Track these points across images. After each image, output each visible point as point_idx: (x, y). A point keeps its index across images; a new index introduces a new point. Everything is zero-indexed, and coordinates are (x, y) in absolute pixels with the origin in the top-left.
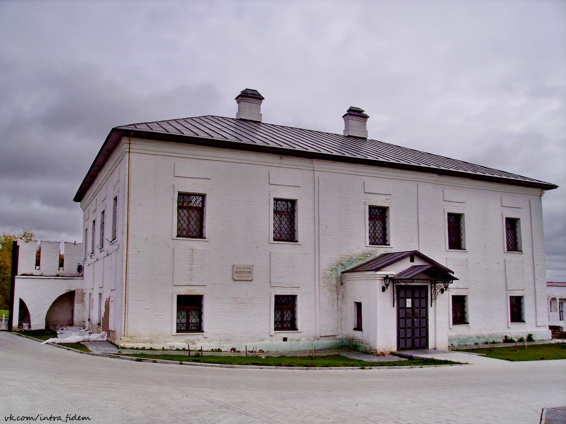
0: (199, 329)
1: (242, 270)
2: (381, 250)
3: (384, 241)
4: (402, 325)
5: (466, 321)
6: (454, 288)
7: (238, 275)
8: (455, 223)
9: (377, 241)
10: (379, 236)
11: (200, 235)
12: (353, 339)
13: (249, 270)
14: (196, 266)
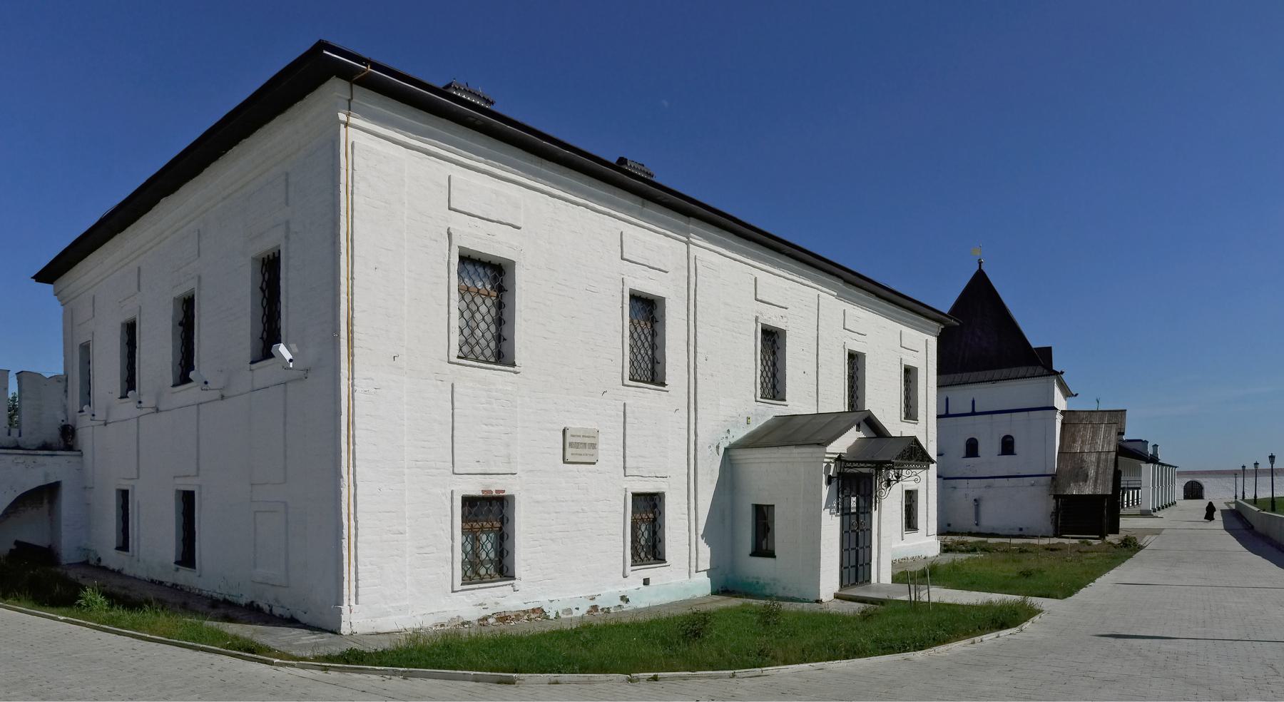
2: (777, 410)
7: (574, 450)
11: (502, 355)
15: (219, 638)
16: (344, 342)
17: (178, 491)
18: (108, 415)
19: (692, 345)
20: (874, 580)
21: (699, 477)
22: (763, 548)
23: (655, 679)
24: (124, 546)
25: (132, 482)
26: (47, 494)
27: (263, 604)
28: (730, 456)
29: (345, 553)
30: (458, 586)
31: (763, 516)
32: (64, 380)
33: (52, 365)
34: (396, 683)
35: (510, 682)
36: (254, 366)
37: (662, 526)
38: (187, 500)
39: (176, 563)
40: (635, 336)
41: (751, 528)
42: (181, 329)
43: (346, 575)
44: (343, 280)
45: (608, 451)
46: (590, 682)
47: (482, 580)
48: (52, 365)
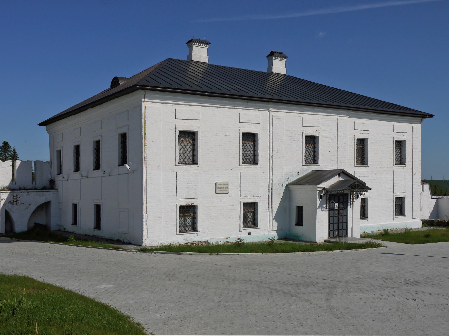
0: (194, 229)
2: (314, 168)
3: (315, 161)
4: (332, 222)
5: (366, 216)
6: (366, 195)
7: (220, 190)
8: (362, 144)
10: (312, 156)
11: (194, 162)
12: (9, 277)
13: (227, 186)
14: (194, 185)
15: (109, 247)
16: (144, 163)
17: (95, 205)
18: (68, 177)
19: (271, 148)
20: (349, 235)
21: (273, 196)
22: (299, 222)
23: (217, 254)
24: (75, 223)
25: (78, 201)
26: (46, 206)
27: (122, 240)
28: (288, 189)
29: (144, 223)
30: (178, 233)
31: (300, 209)
32: (50, 163)
33: (46, 157)
34: (153, 254)
35: (180, 254)
36: (119, 167)
37: (257, 214)
38: (98, 208)
39: (94, 228)
40: (245, 150)
41: (293, 215)
42: (95, 151)
43: (144, 229)
44: (143, 146)
45: (233, 189)
46: (200, 255)
47: (187, 231)
48: (46, 157)
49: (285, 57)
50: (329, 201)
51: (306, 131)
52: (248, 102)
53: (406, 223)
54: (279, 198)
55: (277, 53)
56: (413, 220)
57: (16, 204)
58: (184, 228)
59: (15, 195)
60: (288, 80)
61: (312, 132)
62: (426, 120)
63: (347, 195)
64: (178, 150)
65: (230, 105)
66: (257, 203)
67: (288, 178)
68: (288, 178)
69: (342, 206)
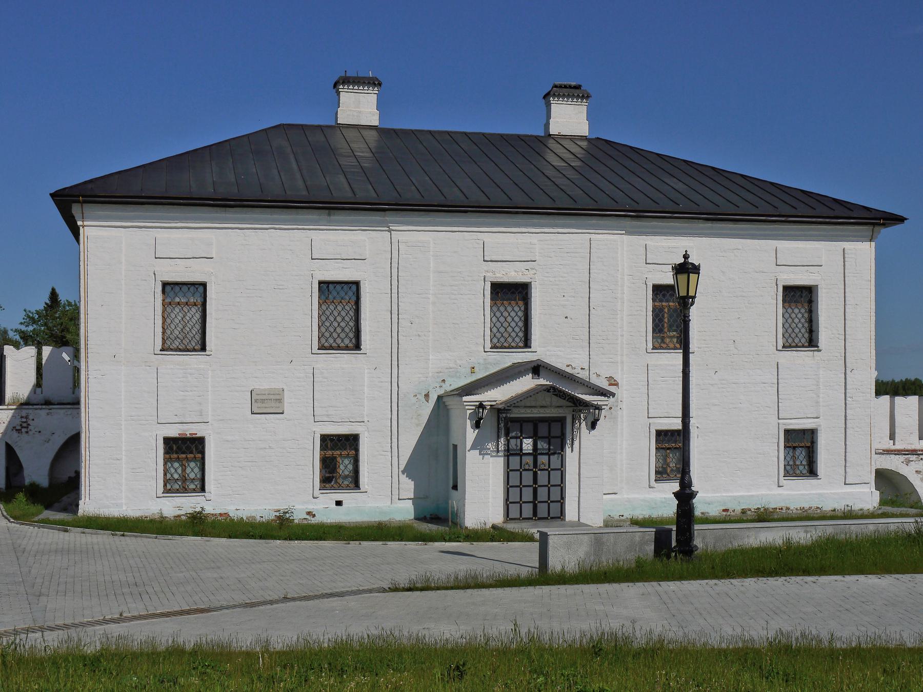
1: (264, 397)
7: (260, 405)
9: (797, 340)
13: (278, 397)
14: (196, 393)
19: (395, 312)
23: (123, 535)
35: (66, 531)
49: (586, 96)
50: (507, 434)
51: (493, 272)
52: (329, 215)
53: (819, 494)
54: (418, 425)
55: (565, 87)
56: (849, 489)
57: (27, 432)
58: (172, 486)
59: (24, 414)
60: (599, 149)
61: (513, 273)
62: (887, 232)
63: (562, 421)
64: (780, 320)
65: (284, 222)
66: (321, 435)
67: (444, 381)
68: (444, 381)
69: (546, 446)
